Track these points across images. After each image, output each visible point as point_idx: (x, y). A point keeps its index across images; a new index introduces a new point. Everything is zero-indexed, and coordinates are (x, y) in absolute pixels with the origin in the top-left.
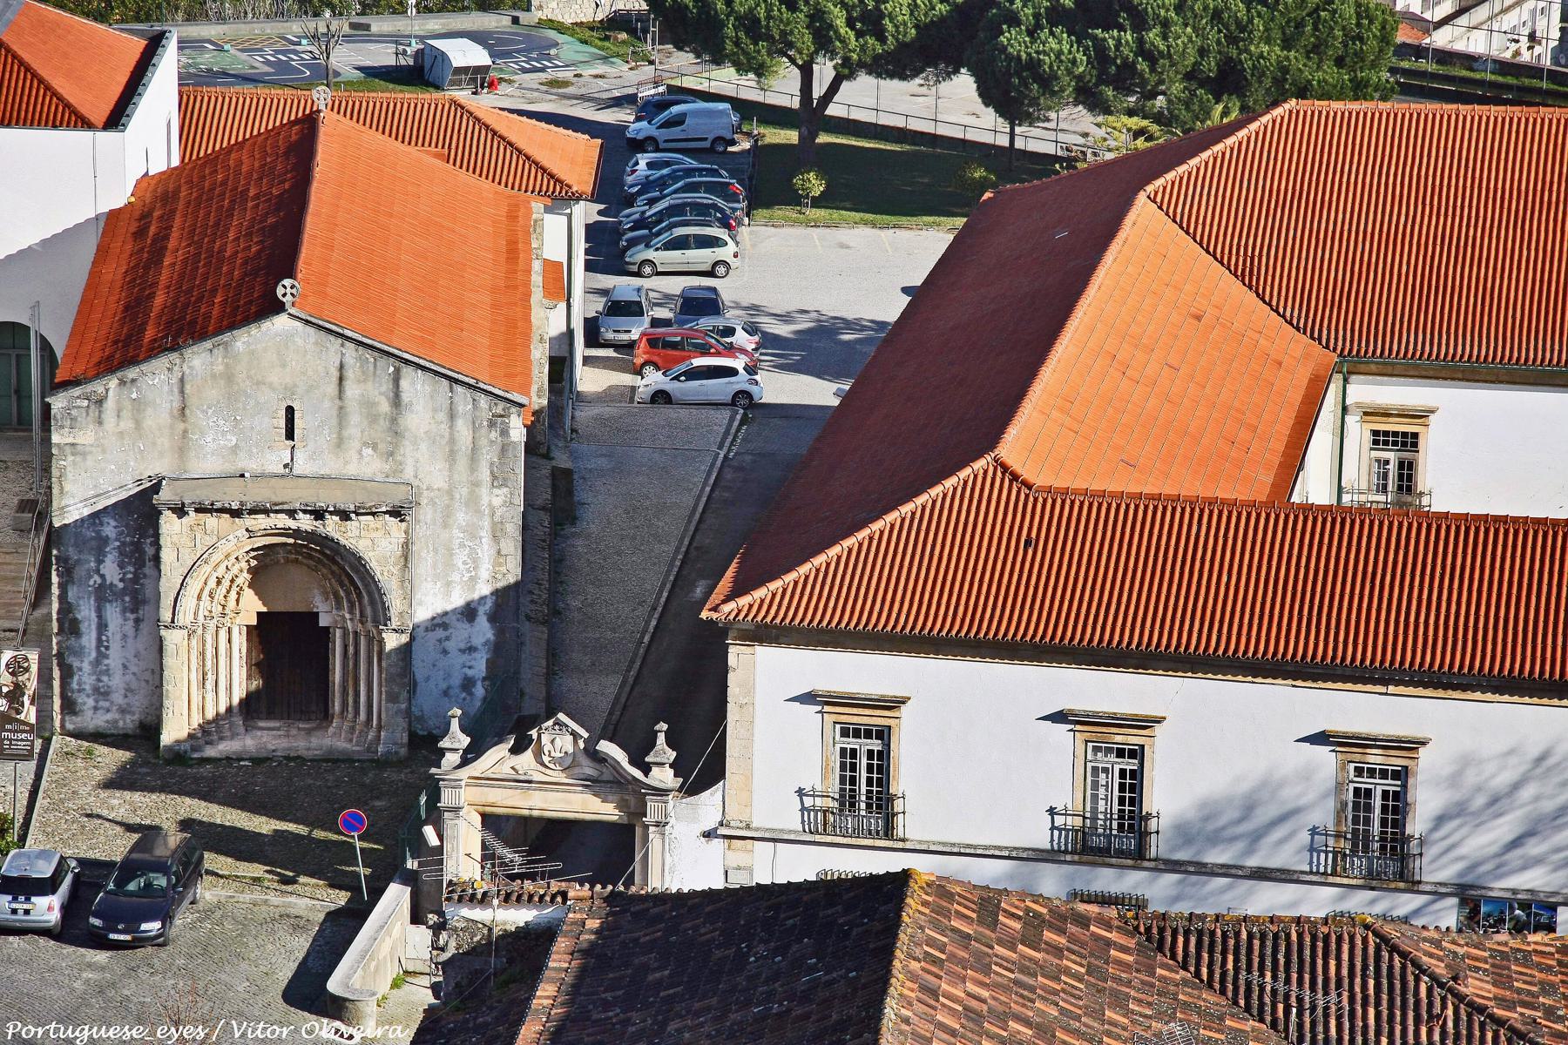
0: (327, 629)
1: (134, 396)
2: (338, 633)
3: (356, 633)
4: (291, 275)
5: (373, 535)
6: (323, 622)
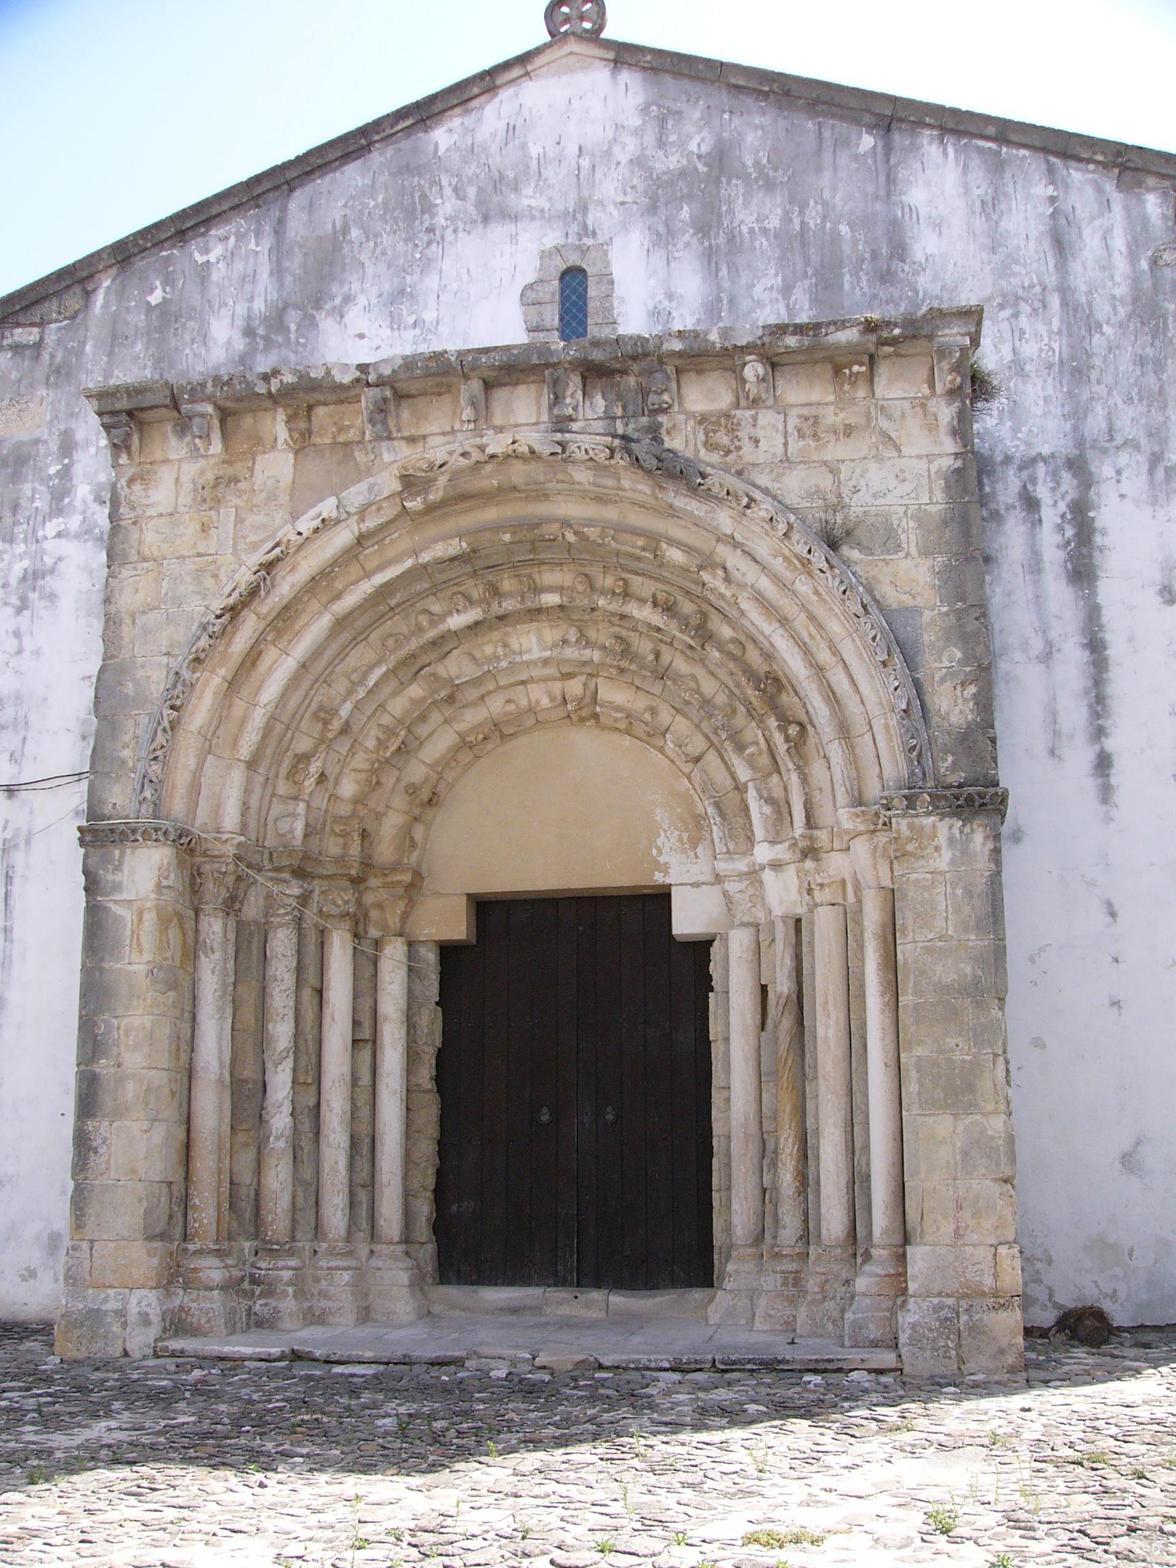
0: (701, 948)
1: (155, 298)
4: (660, 900)
5: (836, 450)
6: (687, 920)
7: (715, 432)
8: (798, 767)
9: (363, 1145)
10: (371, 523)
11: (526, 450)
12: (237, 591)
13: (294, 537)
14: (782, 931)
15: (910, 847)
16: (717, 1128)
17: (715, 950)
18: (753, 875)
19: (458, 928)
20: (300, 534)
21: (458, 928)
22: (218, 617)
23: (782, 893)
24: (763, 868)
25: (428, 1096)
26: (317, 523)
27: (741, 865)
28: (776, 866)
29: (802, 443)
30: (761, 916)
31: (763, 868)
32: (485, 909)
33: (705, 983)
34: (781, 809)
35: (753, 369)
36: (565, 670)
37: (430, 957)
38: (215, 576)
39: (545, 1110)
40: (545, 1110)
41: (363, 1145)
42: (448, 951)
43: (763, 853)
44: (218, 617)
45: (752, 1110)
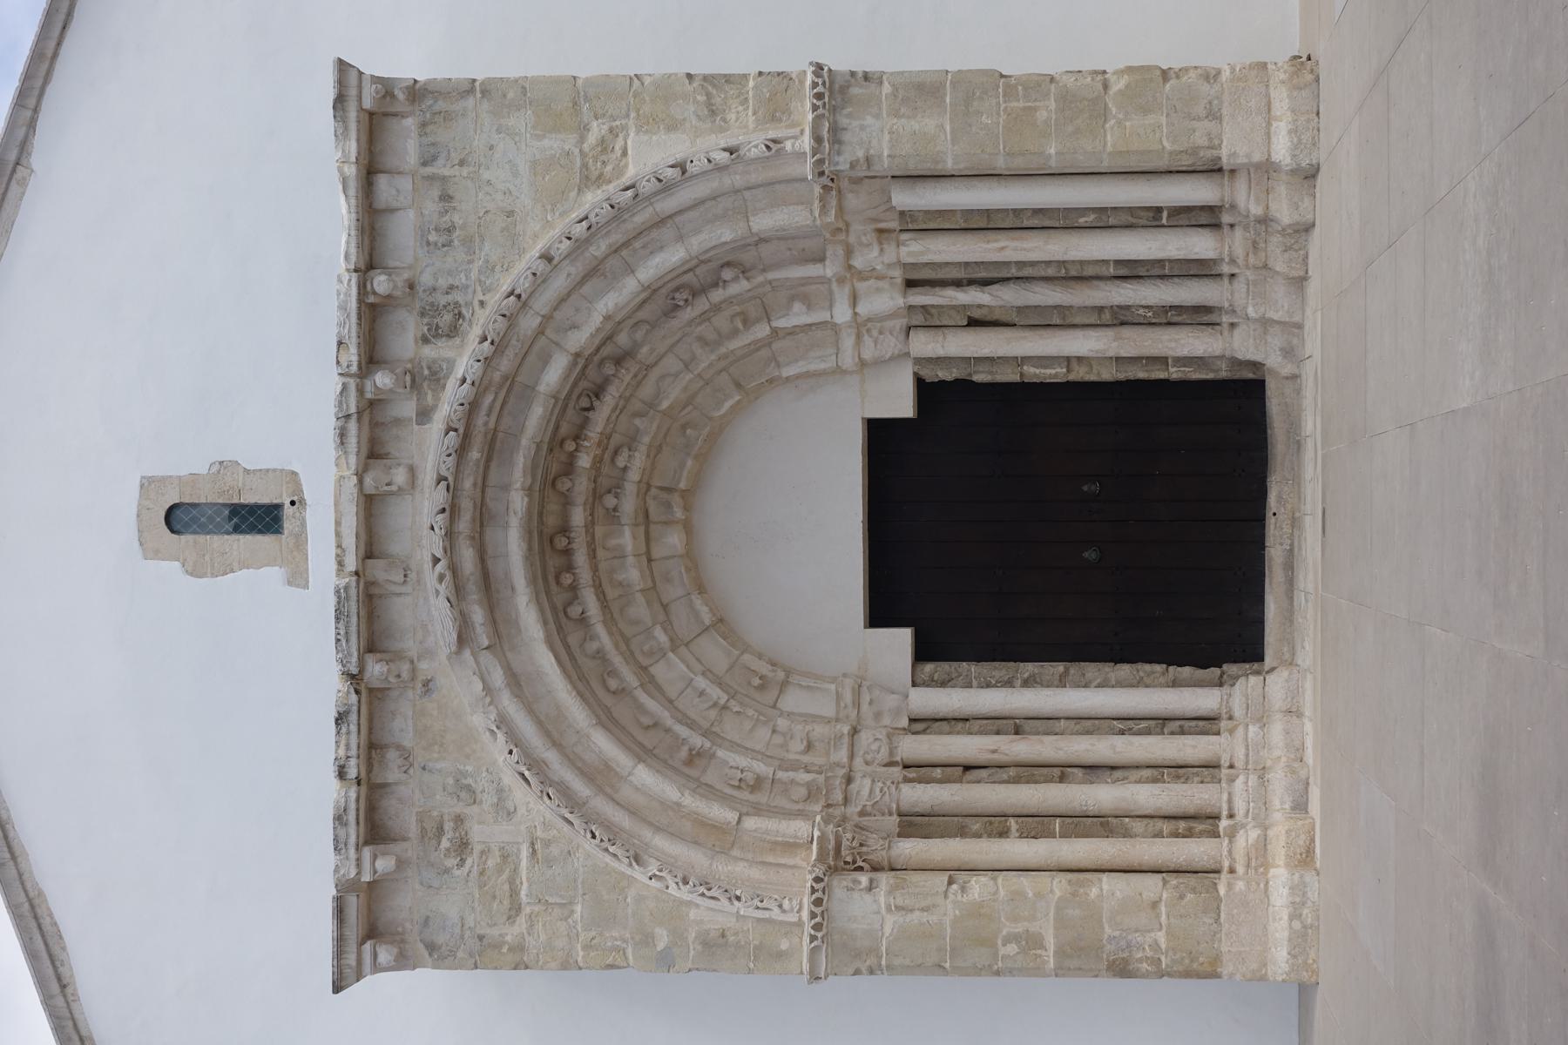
2: (926, 345)
3: (910, 284)
6: (900, 403)
7: (437, 327)
8: (764, 270)
9: (1128, 723)
10: (498, 677)
11: (441, 516)
12: (568, 815)
13: (515, 757)
14: (920, 298)
15: (860, 154)
16: (1107, 374)
17: (930, 375)
18: (861, 326)
19: (902, 638)
20: (511, 752)
21: (902, 638)
22: (594, 837)
23: (885, 300)
24: (856, 314)
25: (1072, 671)
26: (500, 736)
27: (848, 342)
28: (854, 300)
29: (456, 242)
30: (904, 322)
31: (856, 314)
32: (879, 615)
33: (963, 387)
34: (801, 293)
35: (381, 283)
36: (641, 519)
37: (929, 667)
38: (547, 843)
39: (1086, 555)
40: (1086, 555)
41: (1128, 723)
42: (924, 652)
43: (842, 314)
44: (594, 837)
45: (1092, 333)
